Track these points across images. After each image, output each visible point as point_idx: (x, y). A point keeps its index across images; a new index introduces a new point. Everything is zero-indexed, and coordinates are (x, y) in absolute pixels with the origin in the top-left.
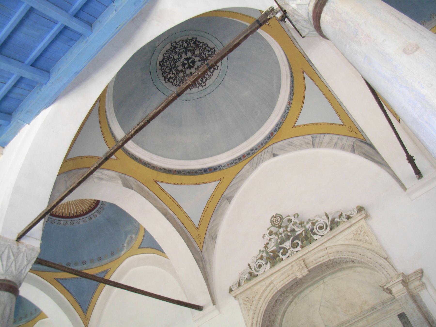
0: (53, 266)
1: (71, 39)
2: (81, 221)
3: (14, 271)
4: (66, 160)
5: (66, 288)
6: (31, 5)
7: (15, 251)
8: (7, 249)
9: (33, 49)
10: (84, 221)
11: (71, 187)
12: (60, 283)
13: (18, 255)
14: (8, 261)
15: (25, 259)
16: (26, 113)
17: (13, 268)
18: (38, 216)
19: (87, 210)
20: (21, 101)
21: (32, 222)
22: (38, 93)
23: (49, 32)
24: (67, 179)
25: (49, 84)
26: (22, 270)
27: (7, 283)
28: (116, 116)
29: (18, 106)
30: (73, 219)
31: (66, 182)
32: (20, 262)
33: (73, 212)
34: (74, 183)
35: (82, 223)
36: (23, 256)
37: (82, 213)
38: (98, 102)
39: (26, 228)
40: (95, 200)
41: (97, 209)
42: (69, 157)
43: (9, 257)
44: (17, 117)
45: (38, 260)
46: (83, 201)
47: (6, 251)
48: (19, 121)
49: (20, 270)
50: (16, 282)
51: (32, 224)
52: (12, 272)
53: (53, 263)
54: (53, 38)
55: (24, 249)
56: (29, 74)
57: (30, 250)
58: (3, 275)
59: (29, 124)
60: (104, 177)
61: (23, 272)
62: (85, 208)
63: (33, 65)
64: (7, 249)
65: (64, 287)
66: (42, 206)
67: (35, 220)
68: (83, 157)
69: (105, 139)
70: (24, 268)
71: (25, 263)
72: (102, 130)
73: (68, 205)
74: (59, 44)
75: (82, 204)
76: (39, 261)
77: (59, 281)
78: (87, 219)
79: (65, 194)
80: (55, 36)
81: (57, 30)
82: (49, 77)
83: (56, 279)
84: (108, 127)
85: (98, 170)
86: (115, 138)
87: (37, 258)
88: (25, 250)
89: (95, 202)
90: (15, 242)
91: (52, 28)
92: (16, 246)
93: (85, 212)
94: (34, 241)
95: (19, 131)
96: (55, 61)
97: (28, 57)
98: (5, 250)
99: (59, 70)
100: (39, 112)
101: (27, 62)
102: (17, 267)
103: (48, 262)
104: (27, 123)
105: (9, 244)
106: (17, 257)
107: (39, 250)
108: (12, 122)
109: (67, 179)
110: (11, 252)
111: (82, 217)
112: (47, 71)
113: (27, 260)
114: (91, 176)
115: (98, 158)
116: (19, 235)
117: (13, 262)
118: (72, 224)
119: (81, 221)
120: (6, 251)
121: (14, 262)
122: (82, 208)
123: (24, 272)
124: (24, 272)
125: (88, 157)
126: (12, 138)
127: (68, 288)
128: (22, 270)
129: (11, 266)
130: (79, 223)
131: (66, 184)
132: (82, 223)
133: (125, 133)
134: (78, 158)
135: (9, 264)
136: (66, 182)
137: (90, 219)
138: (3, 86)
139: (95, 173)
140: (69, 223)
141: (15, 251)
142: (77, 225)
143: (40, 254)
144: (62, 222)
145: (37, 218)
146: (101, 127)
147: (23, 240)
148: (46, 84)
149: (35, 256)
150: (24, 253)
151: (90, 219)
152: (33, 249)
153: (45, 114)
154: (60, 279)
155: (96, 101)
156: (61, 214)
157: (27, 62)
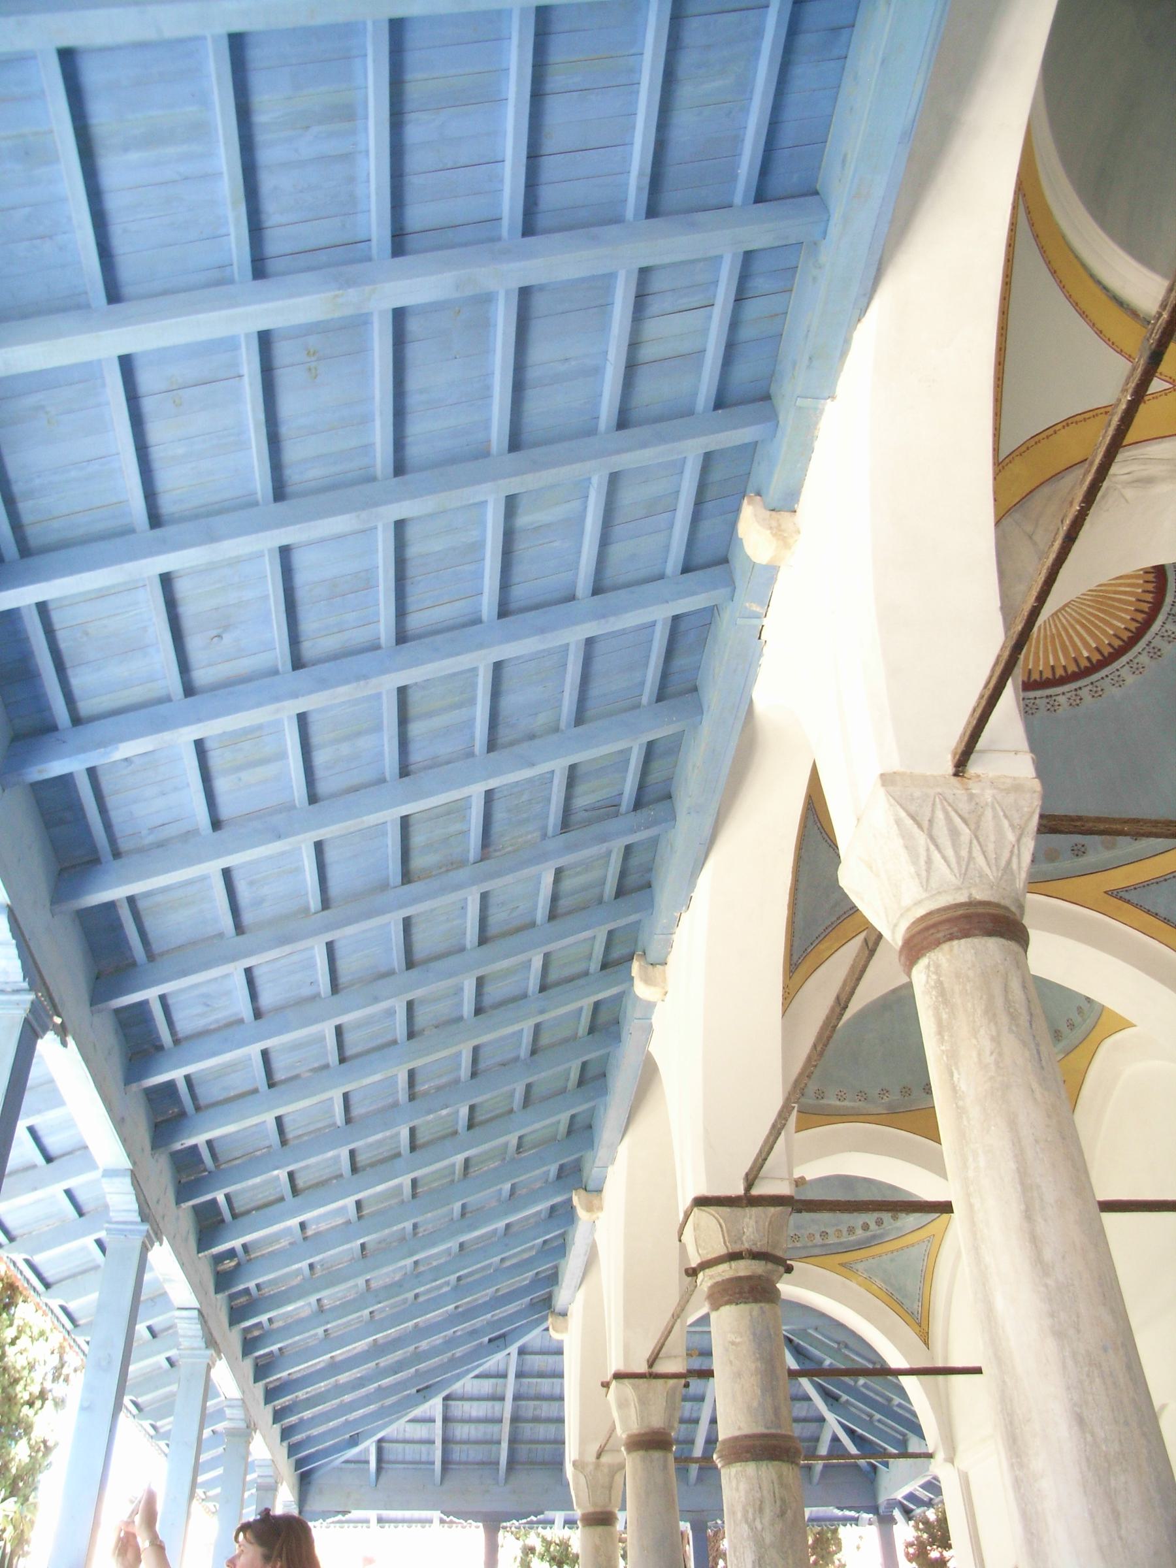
0: (1102, 827)
1: (835, 30)
2: (1125, 672)
3: (987, 870)
4: (1001, 465)
5: (1156, 915)
6: (515, 285)
7: (964, 807)
8: (939, 806)
9: (737, 140)
10: (1137, 669)
11: (1068, 522)
12: (1128, 902)
13: (980, 817)
14: (956, 845)
15: (1006, 823)
16: (808, 367)
17: (980, 860)
18: (993, 671)
19: (1133, 626)
20: (777, 337)
21: (981, 697)
22: (815, 279)
23: (757, 53)
24: (1029, 528)
25: (834, 229)
26: (1009, 862)
27: (980, 910)
28: (1103, 225)
29: (775, 358)
30: (1095, 677)
31: (1030, 537)
32: (992, 838)
33: (1086, 654)
34: (1071, 503)
35: (1130, 679)
36: (995, 817)
37: (1117, 643)
38: (1021, 209)
39: (968, 723)
40: (1146, 572)
41: (1166, 608)
42: (1002, 457)
43: (954, 833)
44: (790, 394)
45: (1045, 822)
46: (1101, 598)
47: (940, 815)
48: (800, 402)
49: (1003, 863)
50: (1006, 902)
51: (984, 702)
52: (982, 875)
53: (1099, 820)
54: (779, 60)
55: (988, 795)
56: (762, 231)
57: (1007, 791)
58: (959, 888)
59: (833, 397)
60: (1153, 470)
61: (1014, 866)
62: (1122, 621)
63: (760, 196)
64: (939, 806)
65: (1148, 912)
66: (988, 641)
67: (986, 687)
68: (1051, 431)
69: (1099, 333)
70: (1012, 852)
71: (1011, 837)
72: (1075, 305)
73: (1060, 635)
74: (804, 73)
75: (1099, 610)
76: (1050, 825)
77: (1126, 896)
78: (1144, 659)
79: (1052, 556)
80: (780, 52)
81: (773, 49)
82: (825, 207)
83: (1113, 894)
84: (1090, 283)
85: (1119, 457)
86: (1133, 313)
87: (1042, 816)
88: (994, 797)
89: (1151, 577)
90: (954, 780)
91: (759, 33)
92: (960, 792)
93: (1126, 635)
94: (1009, 758)
95: (813, 438)
96: (817, 140)
97: (734, 178)
98: (933, 811)
99: (844, 161)
100: (847, 341)
101: (738, 199)
102: (992, 856)
103: (1080, 818)
104: (826, 399)
105: (939, 790)
106: (978, 827)
107: (1037, 785)
108: (781, 418)
109: (1029, 528)
110: (953, 814)
111: (1124, 659)
112: (810, 192)
113: (1012, 825)
114: (1105, 484)
115: (1107, 410)
116: (954, 755)
117: (971, 843)
118: (1097, 694)
119: (1125, 672)
120: (940, 815)
121: (975, 842)
122: (1111, 625)
123: (1019, 868)
124: (1019, 868)
125: (1067, 422)
126: (805, 470)
127: (1163, 913)
128: (1009, 862)
129: (971, 858)
130: (1120, 682)
131: (1035, 544)
132: (1130, 679)
133: (1165, 276)
134: (1036, 439)
135: (964, 853)
136: (1030, 537)
137: (1156, 653)
138: (710, 317)
139: (1114, 469)
140: (1084, 693)
141: (964, 807)
142: (1115, 691)
143: (1046, 796)
144: (1062, 700)
145: (991, 677)
146: (1069, 297)
147: (973, 768)
148: (825, 233)
149: (1030, 806)
150: (993, 808)
151: (1156, 653)
152: (1017, 788)
153: (869, 335)
154: (1126, 889)
155: (1015, 207)
156: (1048, 674)
157: (738, 199)
